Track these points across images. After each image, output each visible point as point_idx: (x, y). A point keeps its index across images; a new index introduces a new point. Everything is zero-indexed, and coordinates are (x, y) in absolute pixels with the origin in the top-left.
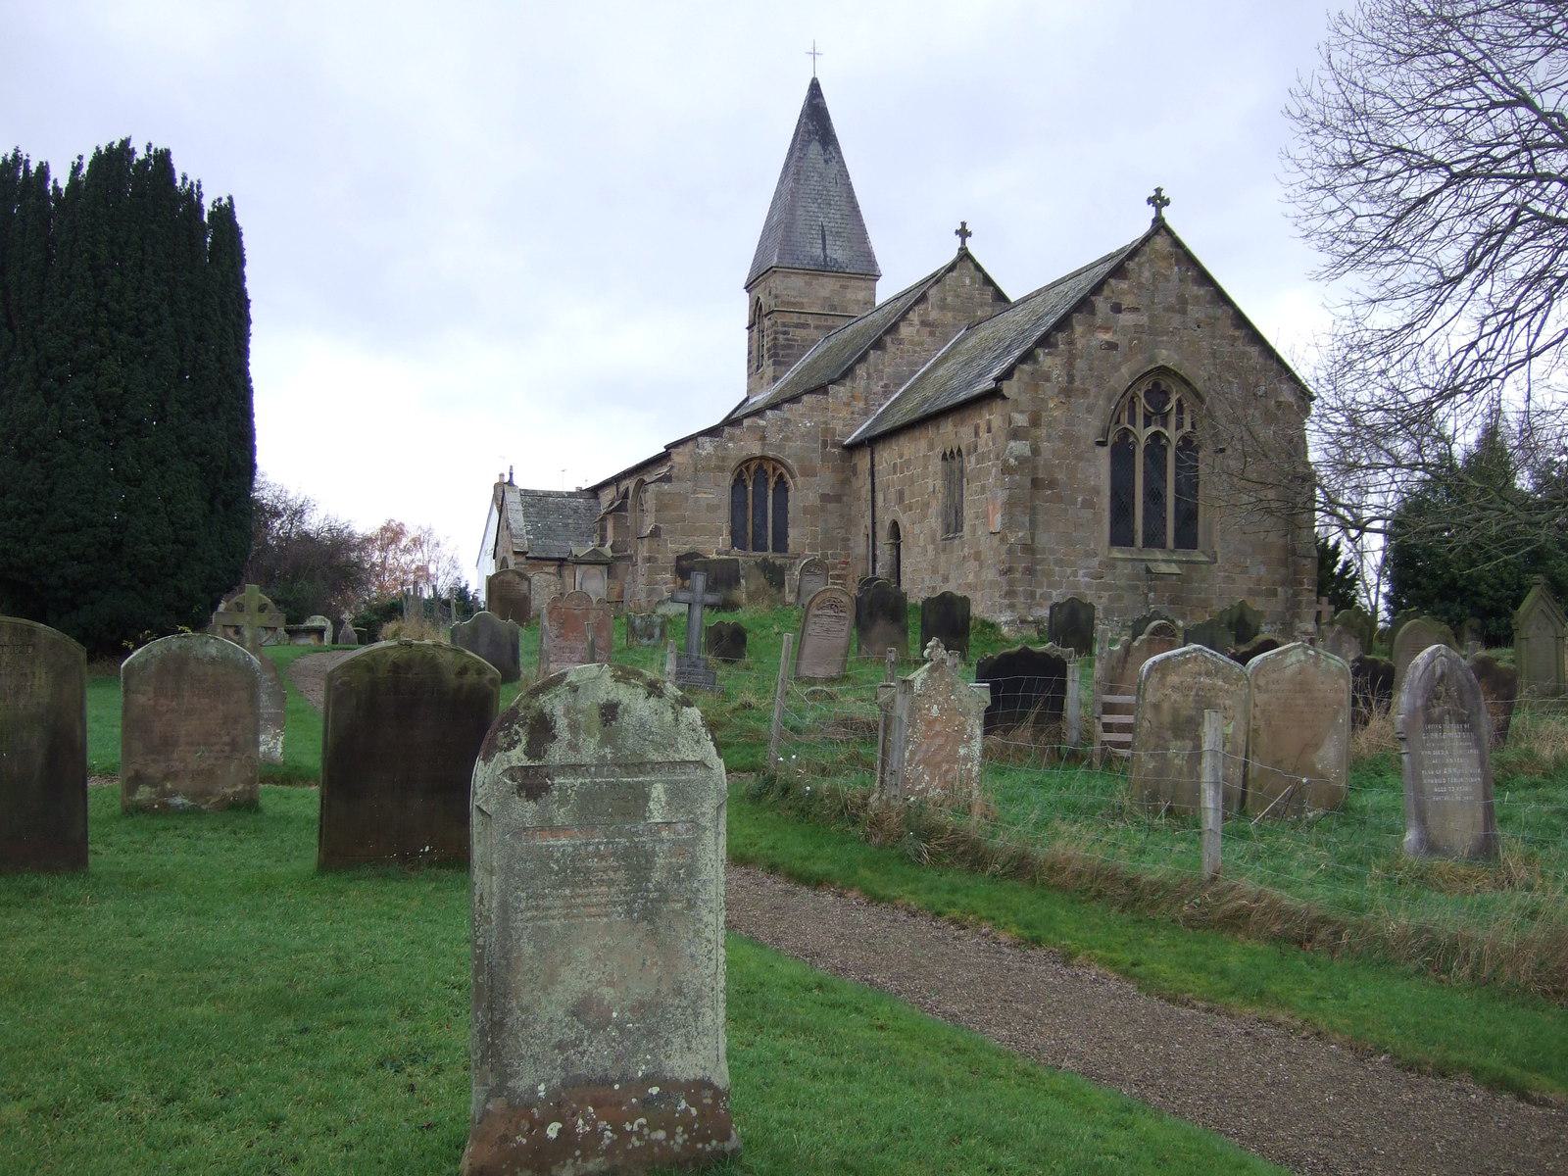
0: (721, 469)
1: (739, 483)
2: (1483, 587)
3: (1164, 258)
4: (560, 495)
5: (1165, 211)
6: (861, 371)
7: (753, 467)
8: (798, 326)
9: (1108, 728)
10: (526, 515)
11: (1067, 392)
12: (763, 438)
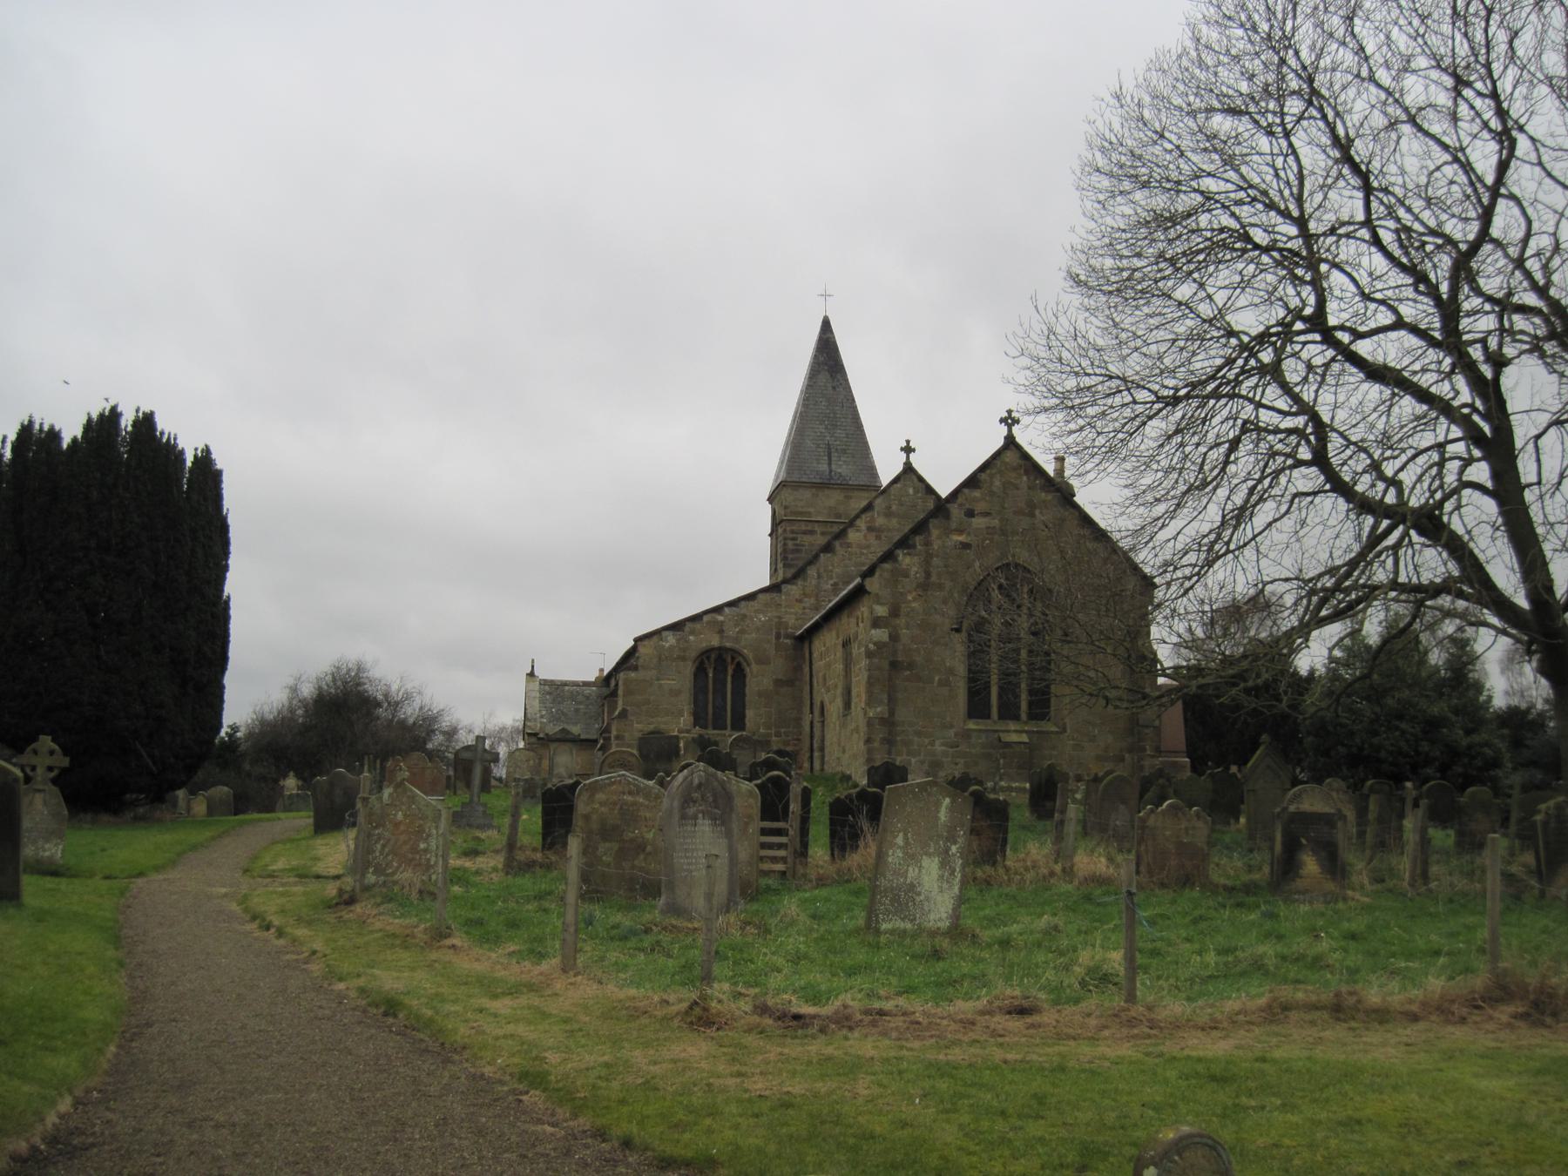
0: (683, 659)
1: (700, 671)
2: (1383, 754)
3: (1015, 469)
4: (575, 684)
5: (1015, 429)
6: (812, 572)
7: (713, 656)
8: (805, 533)
9: (784, 860)
10: (542, 701)
11: (925, 586)
12: (721, 632)
